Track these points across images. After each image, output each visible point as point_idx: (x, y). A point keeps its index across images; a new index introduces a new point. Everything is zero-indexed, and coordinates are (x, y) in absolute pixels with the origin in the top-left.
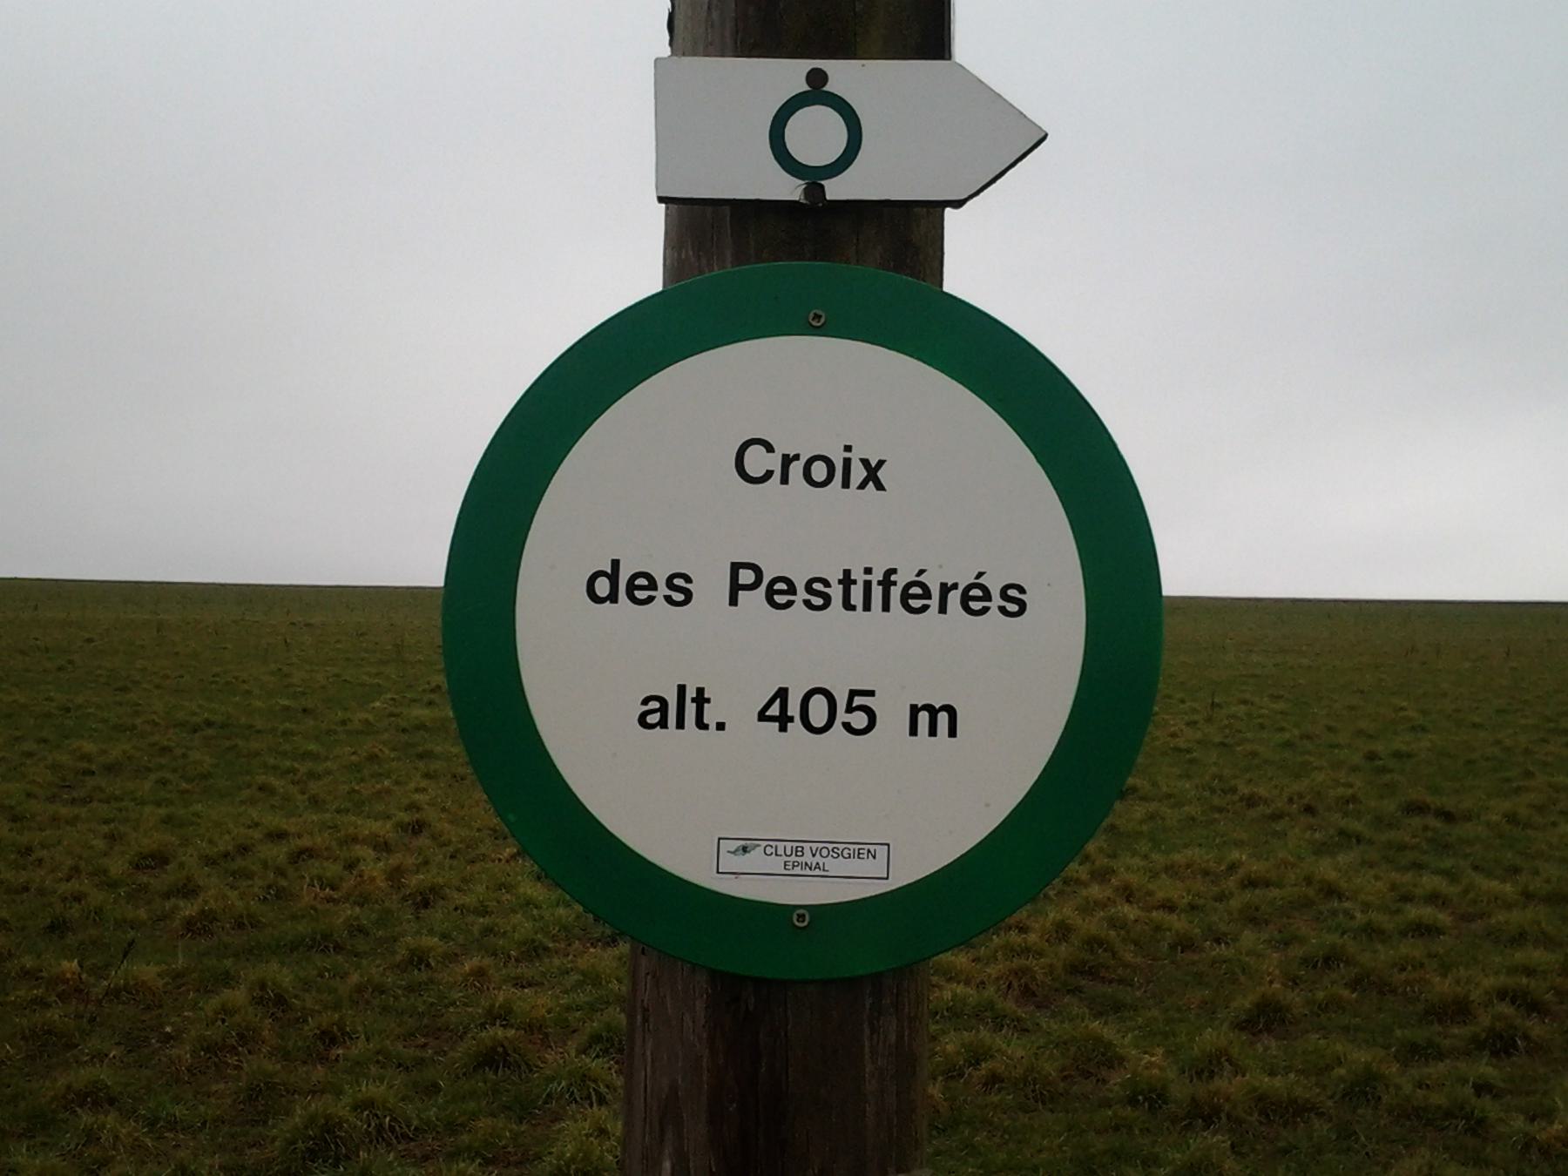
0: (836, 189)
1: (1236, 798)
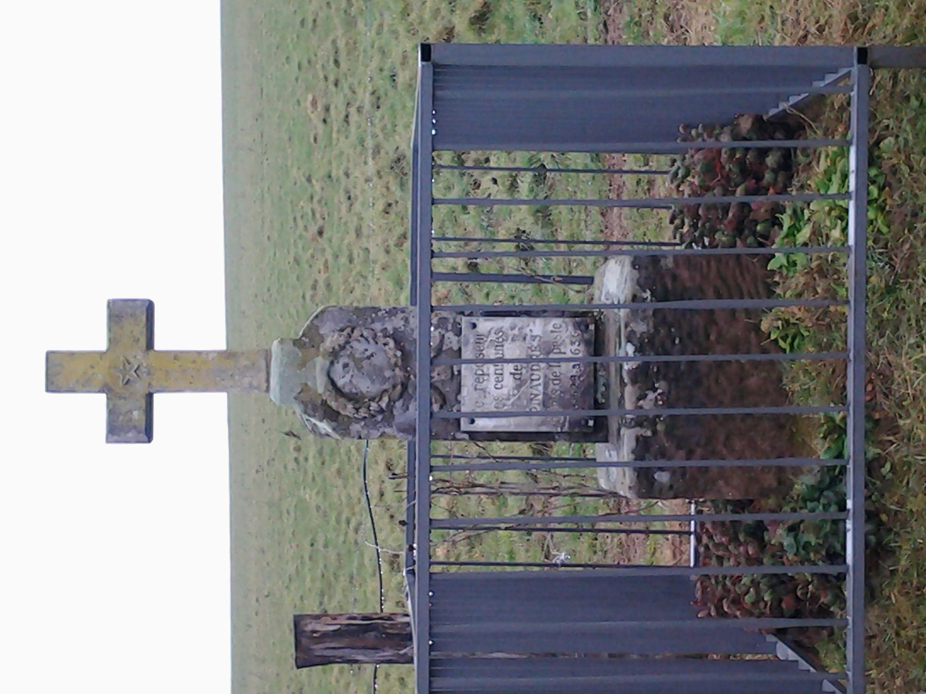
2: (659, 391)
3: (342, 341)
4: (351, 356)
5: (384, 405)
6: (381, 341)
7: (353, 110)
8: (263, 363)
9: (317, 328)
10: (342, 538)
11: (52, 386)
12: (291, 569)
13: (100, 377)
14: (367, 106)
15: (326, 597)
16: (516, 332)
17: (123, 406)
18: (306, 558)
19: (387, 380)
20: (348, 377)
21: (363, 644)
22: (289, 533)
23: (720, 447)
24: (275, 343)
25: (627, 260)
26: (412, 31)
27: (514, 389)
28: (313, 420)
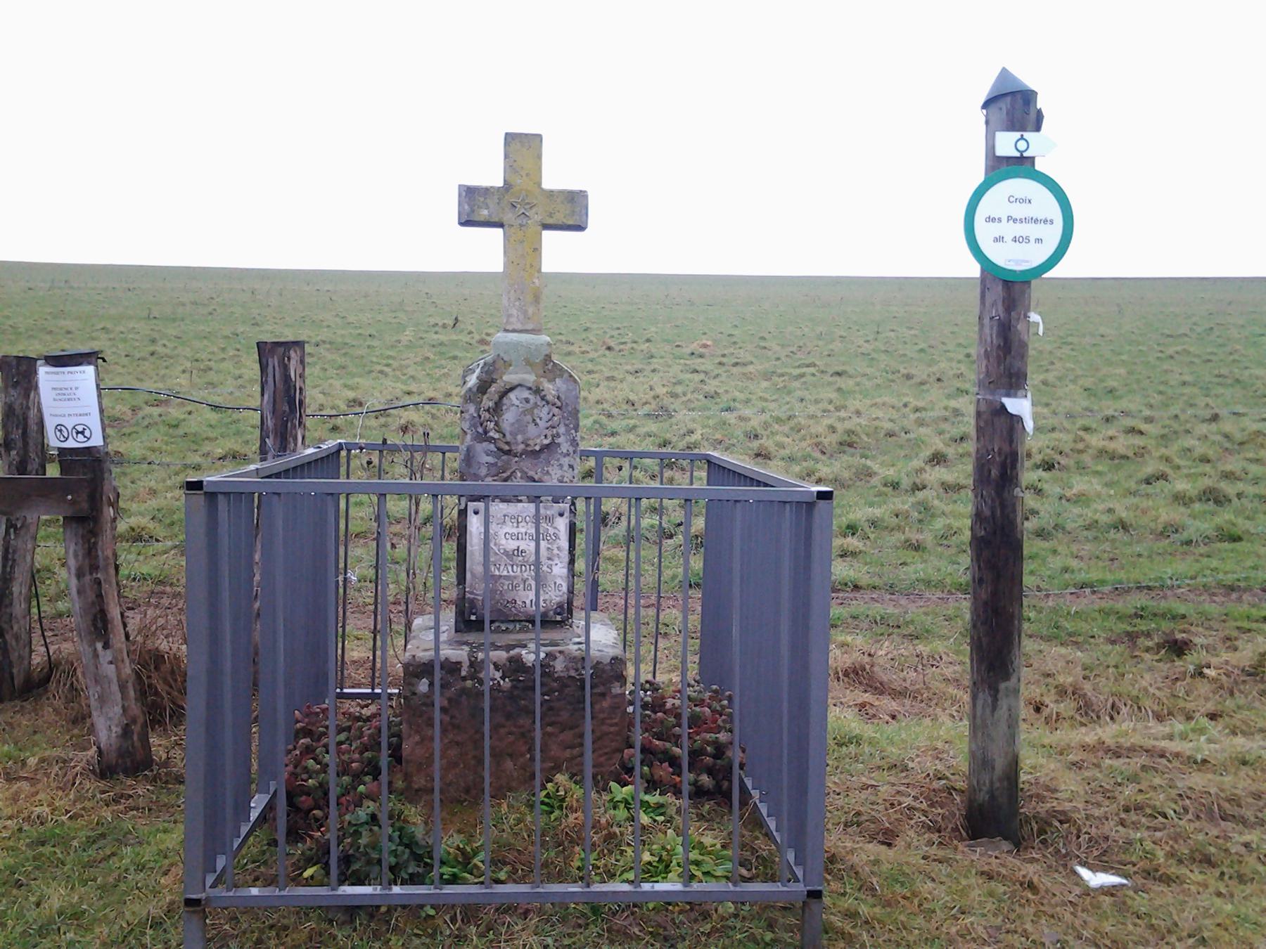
0: (1025, 154)
1: (900, 375)
2: (502, 682)
3: (549, 398)
4: (536, 405)
5: (491, 434)
6: (549, 433)
7: (702, 376)
8: (530, 327)
9: (561, 376)
10: (374, 359)
11: (510, 138)
12: (351, 319)
13: (517, 181)
14: (706, 388)
15: (328, 346)
16: (556, 551)
17: (492, 203)
18: (360, 331)
19: (514, 434)
20: (517, 403)
21: (277, 400)
22: (380, 317)
23: (451, 736)
24: (548, 339)
25: (618, 652)
26: (766, 425)
27: (505, 550)
28: (478, 371)
